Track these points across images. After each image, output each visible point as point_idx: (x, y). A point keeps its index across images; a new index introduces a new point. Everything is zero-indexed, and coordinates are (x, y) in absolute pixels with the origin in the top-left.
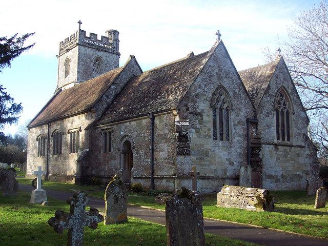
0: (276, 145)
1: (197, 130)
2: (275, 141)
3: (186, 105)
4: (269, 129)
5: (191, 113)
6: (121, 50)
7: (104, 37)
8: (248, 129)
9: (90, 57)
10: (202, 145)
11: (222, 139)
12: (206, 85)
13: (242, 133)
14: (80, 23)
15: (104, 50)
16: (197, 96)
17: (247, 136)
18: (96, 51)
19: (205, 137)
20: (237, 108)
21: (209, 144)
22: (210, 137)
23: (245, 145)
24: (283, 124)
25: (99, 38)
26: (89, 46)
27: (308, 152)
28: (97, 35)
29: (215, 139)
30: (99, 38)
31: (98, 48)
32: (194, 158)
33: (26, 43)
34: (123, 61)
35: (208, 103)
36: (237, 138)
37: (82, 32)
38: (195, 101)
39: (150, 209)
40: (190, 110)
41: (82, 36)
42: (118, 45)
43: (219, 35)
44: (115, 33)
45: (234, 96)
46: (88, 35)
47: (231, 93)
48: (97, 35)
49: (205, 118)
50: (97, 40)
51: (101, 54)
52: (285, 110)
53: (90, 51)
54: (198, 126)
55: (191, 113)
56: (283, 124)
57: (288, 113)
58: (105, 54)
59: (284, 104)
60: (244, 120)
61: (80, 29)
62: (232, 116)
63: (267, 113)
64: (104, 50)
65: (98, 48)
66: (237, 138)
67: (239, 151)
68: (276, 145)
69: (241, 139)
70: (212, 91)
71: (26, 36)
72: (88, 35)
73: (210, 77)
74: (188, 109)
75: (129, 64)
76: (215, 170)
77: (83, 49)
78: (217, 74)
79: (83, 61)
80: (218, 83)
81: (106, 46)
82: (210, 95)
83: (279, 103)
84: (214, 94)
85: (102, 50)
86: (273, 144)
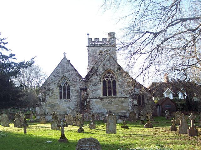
0: (101, 99)
1: (50, 97)
2: (101, 96)
3: (45, 87)
5: (47, 90)
7: (103, 38)
8: (81, 94)
9: (95, 52)
10: (53, 102)
11: (65, 98)
12: (55, 78)
13: (77, 95)
14: (88, 34)
15: (103, 46)
16: (51, 83)
17: (80, 96)
18: (99, 47)
19: (54, 99)
20: (74, 85)
21: (57, 101)
22: (57, 98)
23: (79, 100)
24: (109, 88)
25: (101, 40)
26: (95, 45)
27: (130, 100)
28: (99, 39)
29: (61, 98)
30: (101, 40)
31: (100, 46)
32: (49, 107)
35: (56, 85)
36: (73, 97)
38: (49, 85)
39: (143, 136)
40: (47, 89)
41: (90, 41)
43: (65, 54)
45: (72, 79)
46: (93, 40)
47: (70, 79)
49: (55, 91)
50: (99, 41)
52: (112, 81)
54: (51, 95)
55: (47, 90)
56: (109, 88)
57: (115, 82)
58: (104, 48)
59: (112, 77)
60: (78, 89)
61: (88, 38)
62: (71, 88)
63: (95, 84)
64: (103, 46)
65: (100, 46)
66: (73, 97)
67: (75, 103)
70: (59, 80)
72: (93, 40)
73: (58, 74)
74: (45, 89)
75: (92, 58)
76: (60, 112)
77: (91, 48)
78: (62, 72)
79: (91, 55)
81: (105, 43)
82: (57, 81)
83: (107, 77)
84: (59, 81)
85: (103, 46)
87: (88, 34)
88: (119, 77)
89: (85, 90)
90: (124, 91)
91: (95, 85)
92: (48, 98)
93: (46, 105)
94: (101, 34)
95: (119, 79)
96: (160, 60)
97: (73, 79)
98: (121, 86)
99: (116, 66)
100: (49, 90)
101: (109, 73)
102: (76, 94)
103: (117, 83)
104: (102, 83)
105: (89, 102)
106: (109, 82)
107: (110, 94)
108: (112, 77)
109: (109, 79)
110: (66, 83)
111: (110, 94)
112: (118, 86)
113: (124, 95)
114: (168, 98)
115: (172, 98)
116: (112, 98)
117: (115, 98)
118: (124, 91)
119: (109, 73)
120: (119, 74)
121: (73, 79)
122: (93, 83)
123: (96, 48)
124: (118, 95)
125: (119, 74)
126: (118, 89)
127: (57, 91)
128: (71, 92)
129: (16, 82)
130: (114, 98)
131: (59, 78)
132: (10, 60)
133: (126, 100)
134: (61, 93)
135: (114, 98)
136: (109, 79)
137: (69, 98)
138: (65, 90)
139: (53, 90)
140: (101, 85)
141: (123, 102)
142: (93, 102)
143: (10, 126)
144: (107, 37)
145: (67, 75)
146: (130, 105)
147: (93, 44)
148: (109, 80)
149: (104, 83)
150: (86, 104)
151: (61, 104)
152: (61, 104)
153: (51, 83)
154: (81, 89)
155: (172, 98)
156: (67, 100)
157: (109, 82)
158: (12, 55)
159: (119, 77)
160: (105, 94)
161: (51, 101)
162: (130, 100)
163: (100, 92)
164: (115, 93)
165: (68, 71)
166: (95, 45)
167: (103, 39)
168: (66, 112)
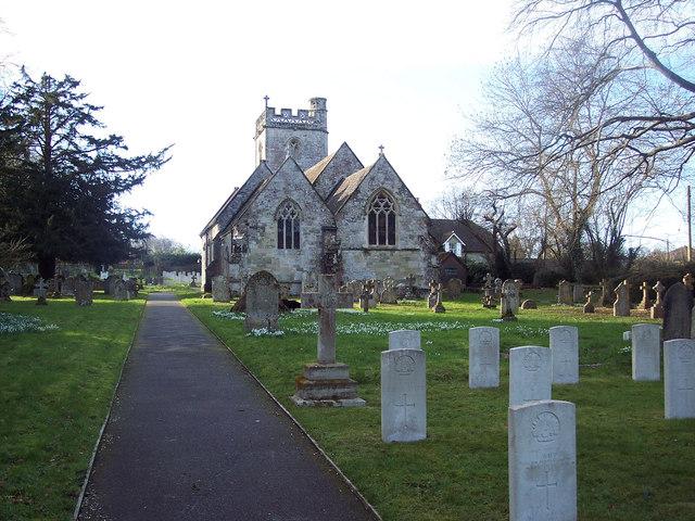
0: (366, 251)
1: (258, 242)
2: (366, 246)
4: (356, 231)
6: (331, 125)
8: (323, 237)
11: (289, 247)
14: (267, 98)
15: (302, 127)
16: (259, 212)
17: (322, 244)
21: (273, 253)
24: (382, 228)
25: (295, 113)
26: (281, 125)
27: (423, 255)
28: (290, 110)
29: (280, 247)
30: (295, 113)
31: (293, 127)
33: (167, 155)
34: (333, 147)
37: (270, 110)
42: (324, 120)
44: (320, 104)
46: (278, 112)
47: (302, 205)
48: (290, 110)
49: (268, 230)
50: (291, 117)
51: (297, 134)
52: (387, 214)
53: (281, 133)
56: (382, 228)
57: (392, 217)
58: (303, 132)
59: (387, 205)
60: (319, 228)
62: (303, 226)
64: (302, 127)
65: (293, 127)
67: (310, 258)
68: (366, 251)
69: (315, 246)
71: (166, 149)
80: (284, 197)
82: (274, 209)
83: (377, 205)
84: (278, 209)
86: (362, 249)
87: (267, 98)
88: (402, 206)
89: (334, 230)
90: (411, 237)
91: (353, 220)
92: (253, 245)
93: (249, 262)
94: (296, 100)
95: (402, 210)
96: (672, 188)
97: (308, 206)
98: (405, 225)
99: (397, 182)
100: (256, 228)
101: (381, 197)
102: (313, 238)
103: (398, 219)
104: (367, 217)
105: (340, 257)
106: (382, 215)
107: (382, 241)
108: (387, 205)
109: (382, 209)
110: (293, 214)
111: (382, 241)
112: (398, 225)
113: (411, 246)
114: (452, 254)
115: (459, 253)
116: (386, 250)
117: (394, 250)
118: (411, 237)
119: (381, 197)
120: (402, 200)
121: (308, 206)
122: (350, 215)
123: (285, 131)
124: (399, 244)
125: (402, 200)
126: (400, 231)
127: (272, 230)
128: (302, 233)
129: (123, 202)
130: (391, 250)
131: (277, 202)
132: (111, 149)
133: (415, 254)
134: (280, 235)
135: (391, 250)
136: (382, 209)
137: (297, 246)
138: (289, 230)
139: (263, 228)
140: (366, 222)
141: (408, 259)
142: (349, 256)
143: (655, 376)
144: (308, 106)
145: (295, 196)
146: (423, 265)
147: (275, 122)
148: (382, 213)
149: (372, 216)
150: (335, 261)
151: (281, 258)
152: (281, 258)
153: (259, 212)
154: (325, 229)
155: (459, 253)
156: (293, 250)
157: (382, 215)
158: (115, 140)
159: (402, 206)
160: (372, 241)
161: (260, 251)
162: (423, 255)
163: (363, 237)
164: (392, 241)
165: (297, 188)
166: (281, 125)
167: (300, 111)
168: (292, 276)
